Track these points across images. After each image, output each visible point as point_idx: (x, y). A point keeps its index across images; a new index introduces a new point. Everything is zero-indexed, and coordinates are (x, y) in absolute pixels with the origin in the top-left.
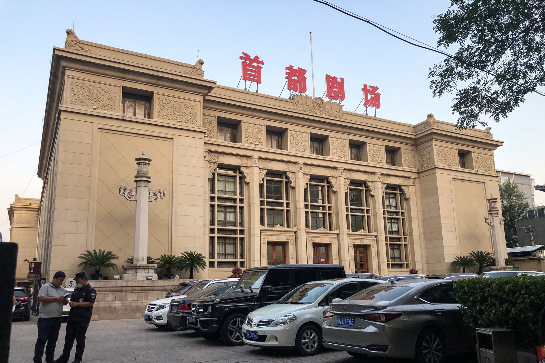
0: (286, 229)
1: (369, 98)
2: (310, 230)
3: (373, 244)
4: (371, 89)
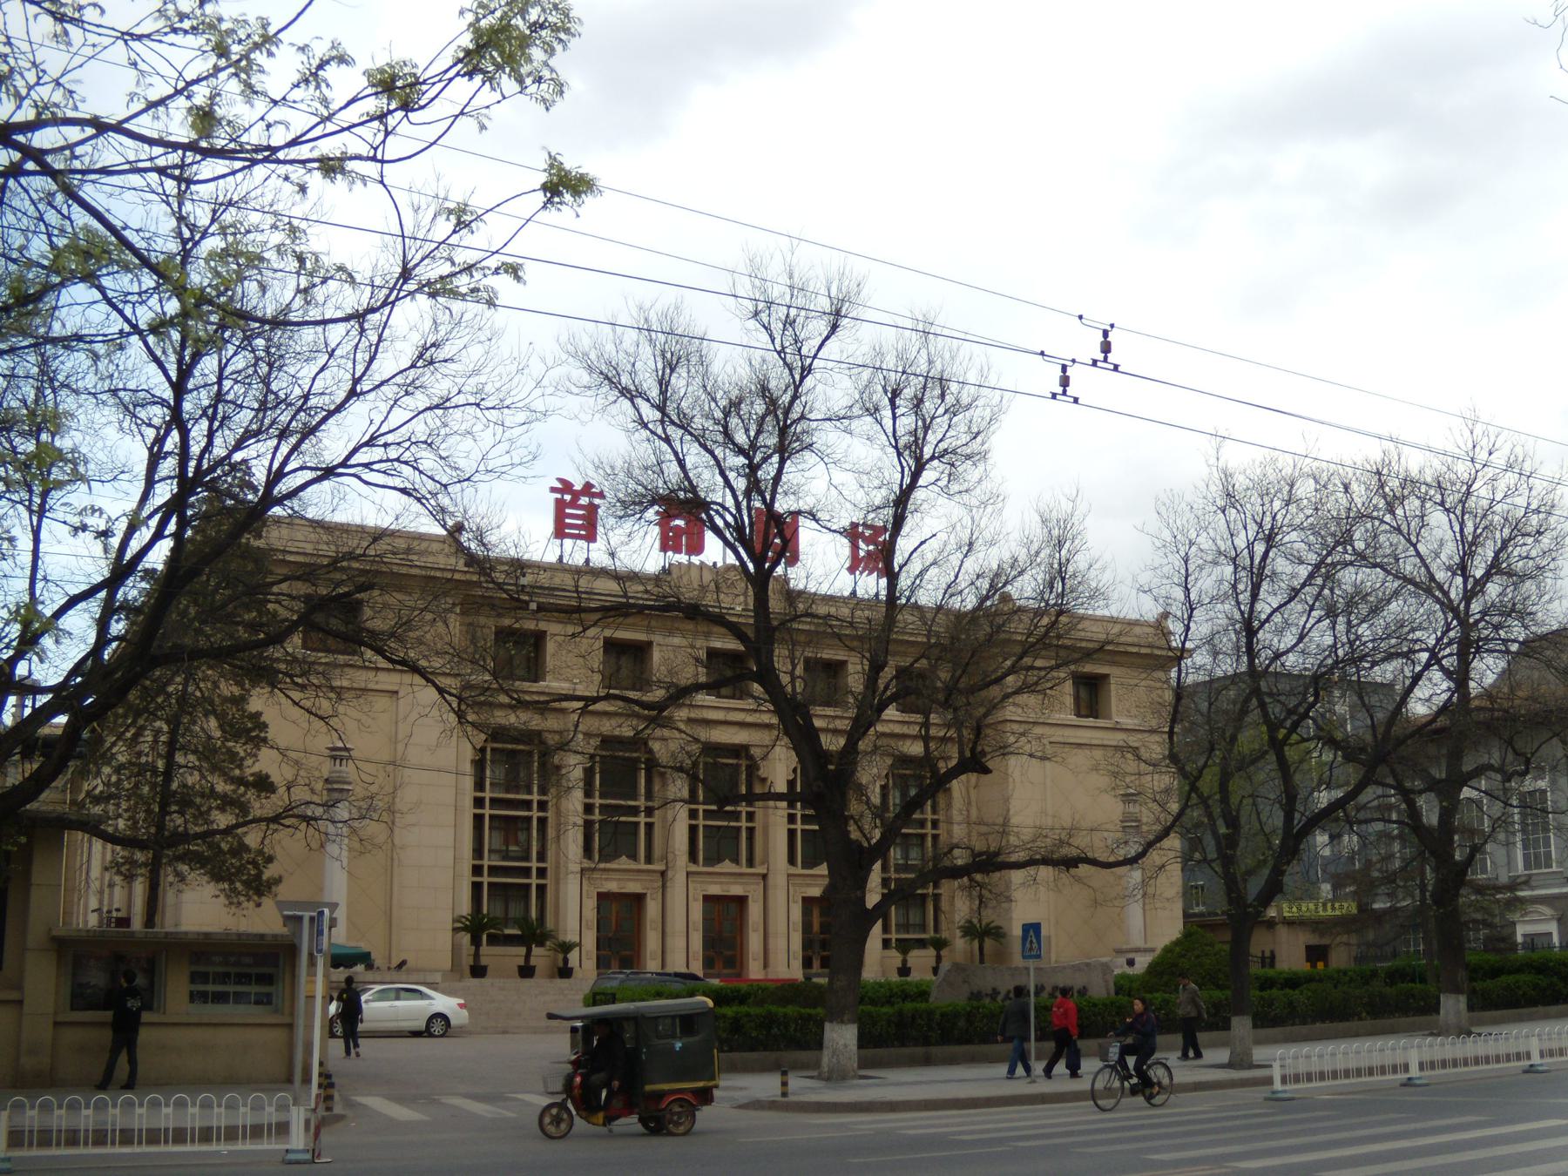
0: (644, 867)
1: (862, 554)
2: (799, 870)
3: (753, 891)
4: (868, 533)
